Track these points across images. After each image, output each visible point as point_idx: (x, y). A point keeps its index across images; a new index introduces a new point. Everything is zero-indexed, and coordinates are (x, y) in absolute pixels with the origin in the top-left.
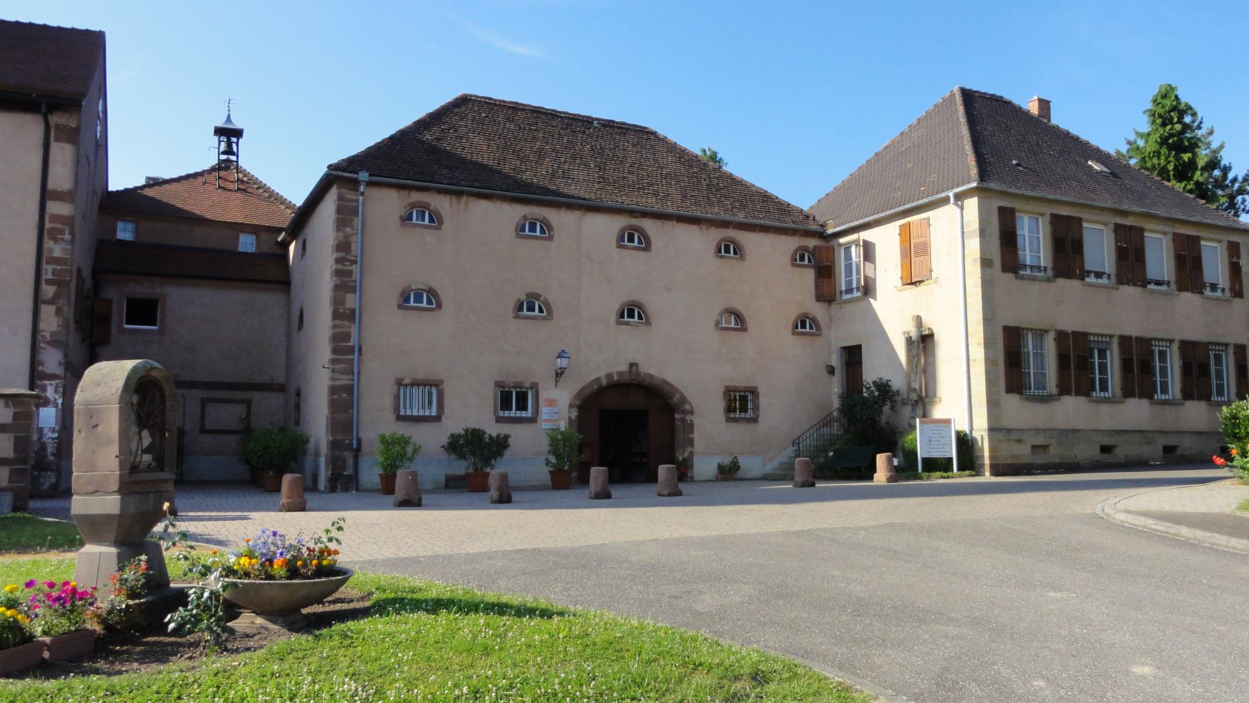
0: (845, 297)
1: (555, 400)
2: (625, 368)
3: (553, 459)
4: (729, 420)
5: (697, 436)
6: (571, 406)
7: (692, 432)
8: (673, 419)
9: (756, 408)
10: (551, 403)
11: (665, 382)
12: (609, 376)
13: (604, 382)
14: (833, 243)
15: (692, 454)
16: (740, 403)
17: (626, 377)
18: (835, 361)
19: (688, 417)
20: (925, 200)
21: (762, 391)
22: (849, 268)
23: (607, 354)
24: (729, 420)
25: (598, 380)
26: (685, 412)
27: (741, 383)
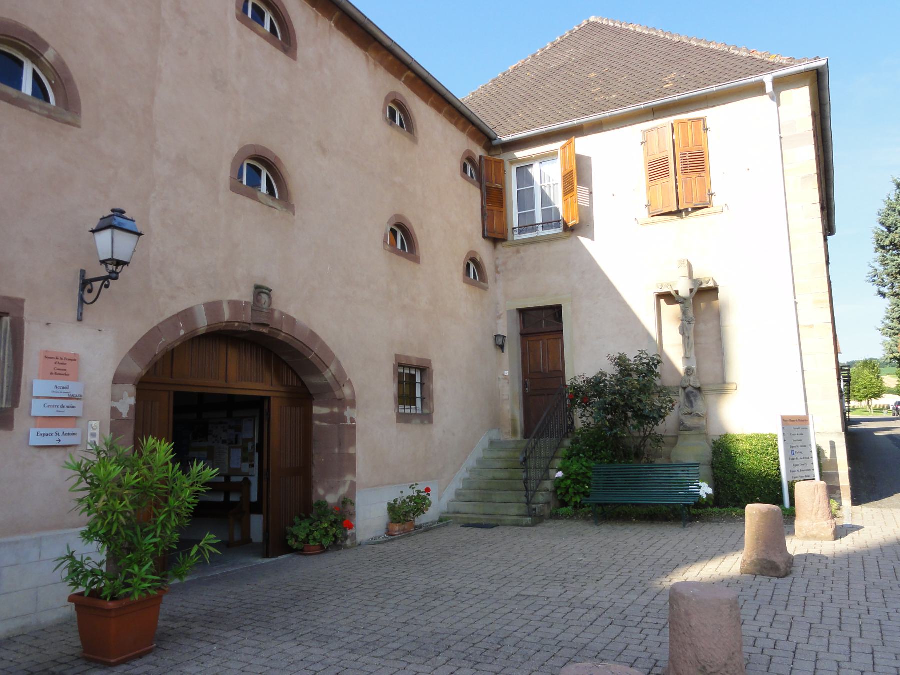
0: (517, 237)
1: (74, 359)
2: (245, 295)
3: (94, 554)
4: (403, 418)
5: (361, 451)
6: (118, 379)
7: (353, 442)
8: (308, 417)
9: (427, 398)
10: (62, 366)
11: (313, 335)
12: (213, 308)
13: (203, 323)
14: (505, 157)
15: (353, 485)
16: (412, 384)
17: (247, 317)
18: (507, 327)
19: (349, 413)
20: (714, 88)
21: (436, 367)
22: (526, 199)
23: (207, 261)
24: (403, 418)
25: (187, 315)
26: (343, 403)
27: (414, 354)
